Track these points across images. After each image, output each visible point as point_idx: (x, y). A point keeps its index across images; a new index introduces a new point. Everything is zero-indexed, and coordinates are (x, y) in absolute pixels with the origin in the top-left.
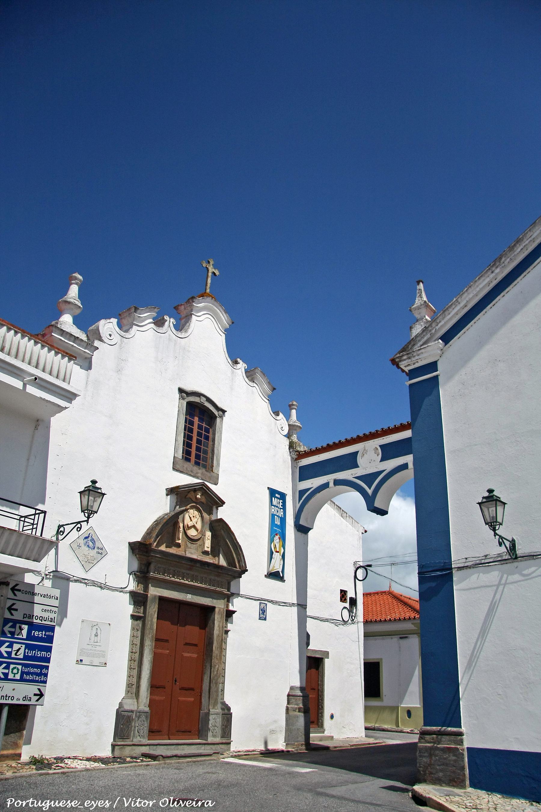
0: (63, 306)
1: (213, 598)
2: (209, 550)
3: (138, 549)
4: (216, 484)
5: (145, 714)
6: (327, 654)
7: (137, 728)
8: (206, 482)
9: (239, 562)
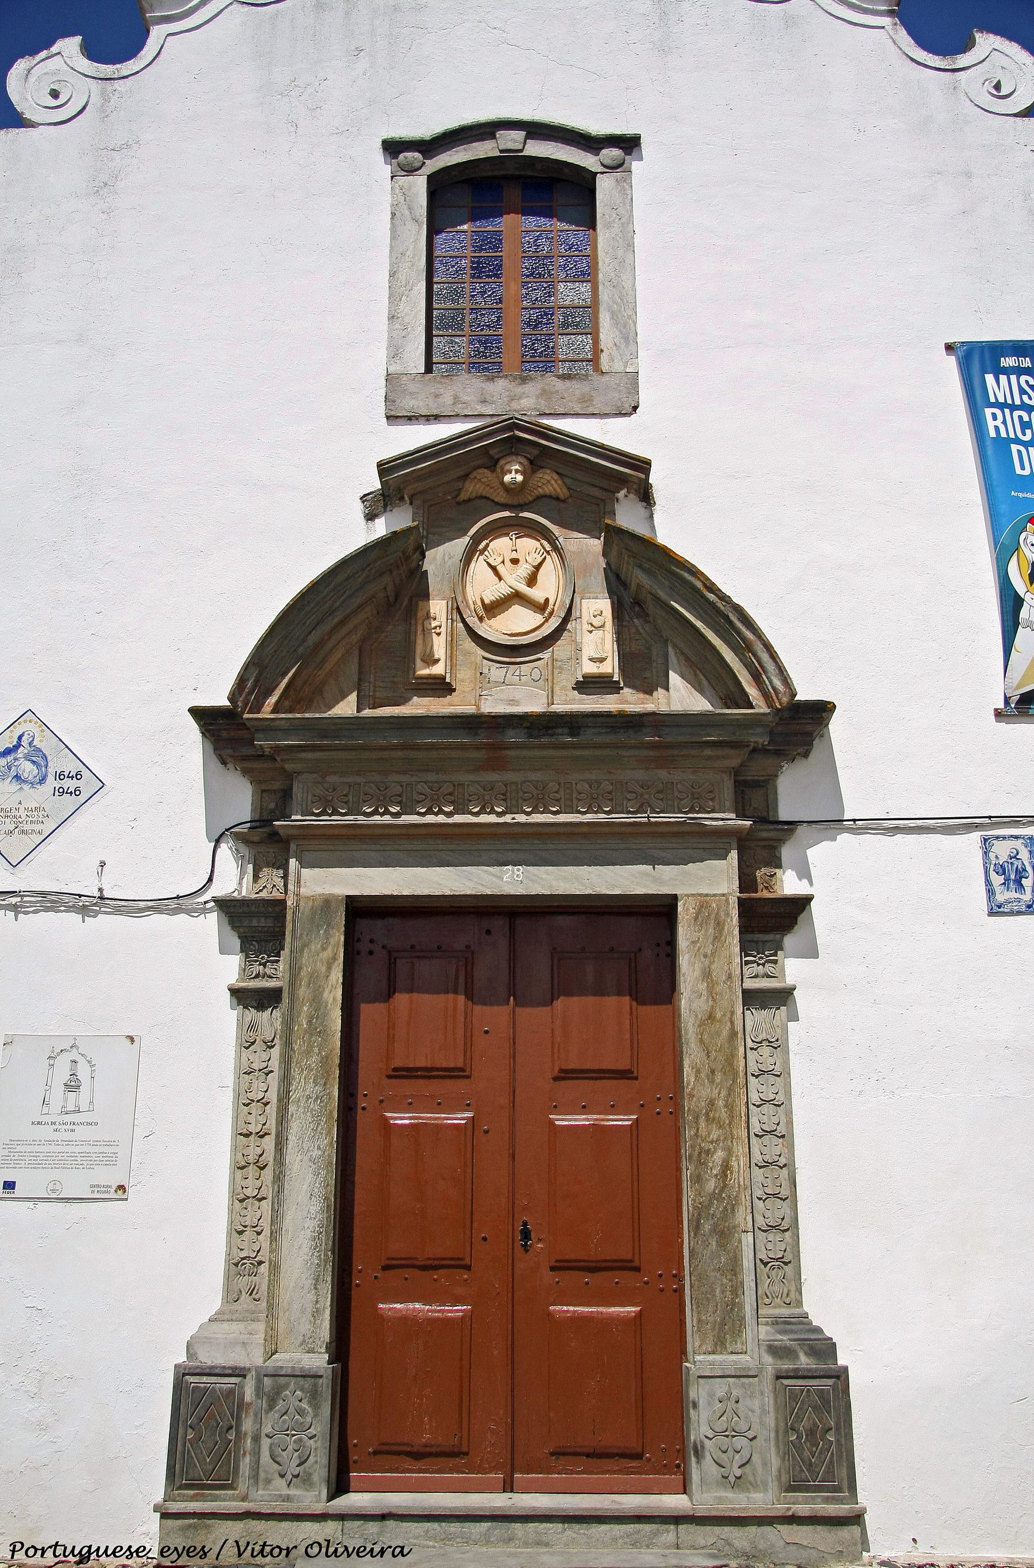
1: (654, 862)
2: (610, 667)
3: (221, 729)
5: (308, 1384)
7: (265, 1443)
9: (757, 678)
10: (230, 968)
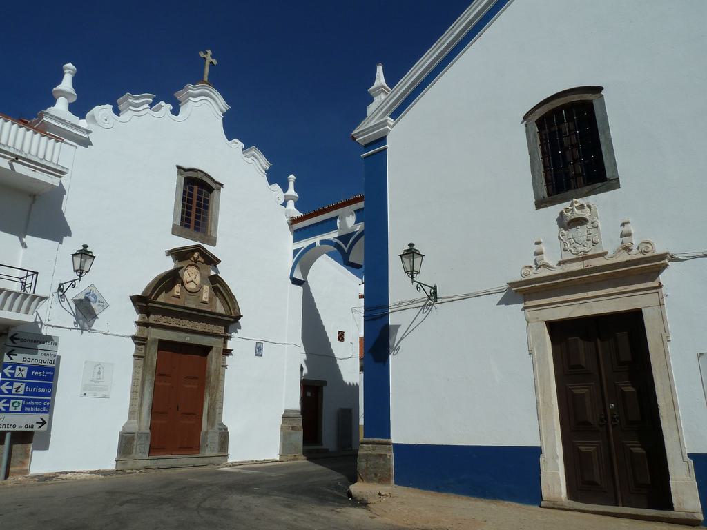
0: (55, 95)
3: (140, 302)
4: (214, 245)
6: (325, 383)
8: (204, 245)
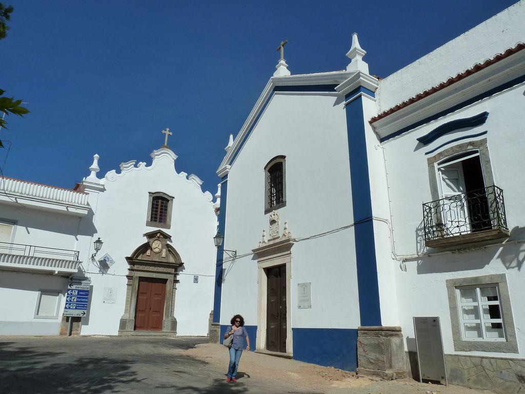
10: (129, 267)
